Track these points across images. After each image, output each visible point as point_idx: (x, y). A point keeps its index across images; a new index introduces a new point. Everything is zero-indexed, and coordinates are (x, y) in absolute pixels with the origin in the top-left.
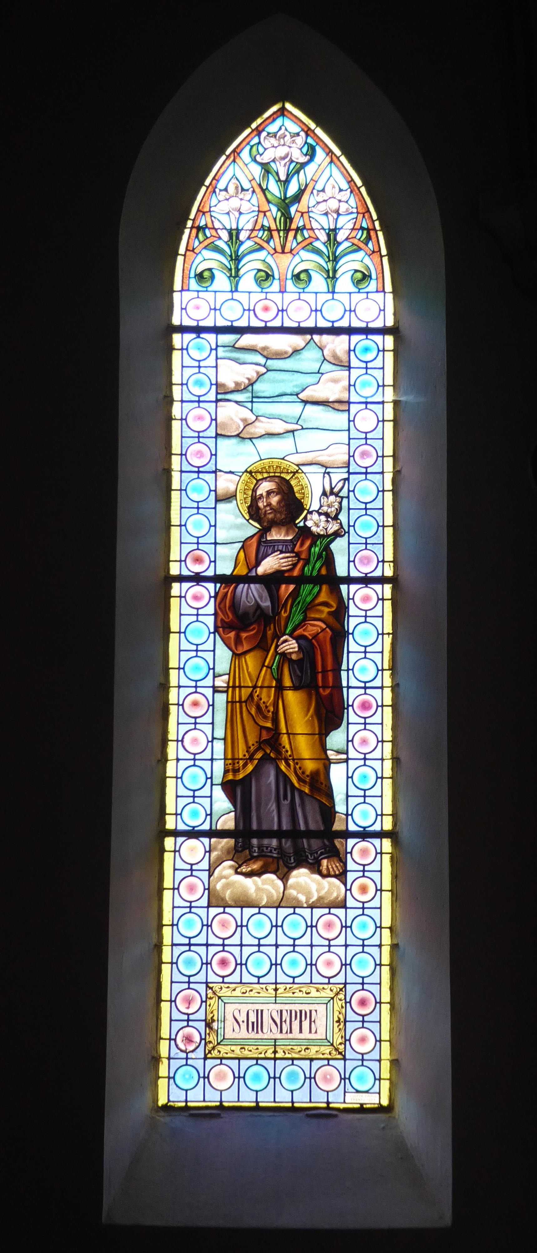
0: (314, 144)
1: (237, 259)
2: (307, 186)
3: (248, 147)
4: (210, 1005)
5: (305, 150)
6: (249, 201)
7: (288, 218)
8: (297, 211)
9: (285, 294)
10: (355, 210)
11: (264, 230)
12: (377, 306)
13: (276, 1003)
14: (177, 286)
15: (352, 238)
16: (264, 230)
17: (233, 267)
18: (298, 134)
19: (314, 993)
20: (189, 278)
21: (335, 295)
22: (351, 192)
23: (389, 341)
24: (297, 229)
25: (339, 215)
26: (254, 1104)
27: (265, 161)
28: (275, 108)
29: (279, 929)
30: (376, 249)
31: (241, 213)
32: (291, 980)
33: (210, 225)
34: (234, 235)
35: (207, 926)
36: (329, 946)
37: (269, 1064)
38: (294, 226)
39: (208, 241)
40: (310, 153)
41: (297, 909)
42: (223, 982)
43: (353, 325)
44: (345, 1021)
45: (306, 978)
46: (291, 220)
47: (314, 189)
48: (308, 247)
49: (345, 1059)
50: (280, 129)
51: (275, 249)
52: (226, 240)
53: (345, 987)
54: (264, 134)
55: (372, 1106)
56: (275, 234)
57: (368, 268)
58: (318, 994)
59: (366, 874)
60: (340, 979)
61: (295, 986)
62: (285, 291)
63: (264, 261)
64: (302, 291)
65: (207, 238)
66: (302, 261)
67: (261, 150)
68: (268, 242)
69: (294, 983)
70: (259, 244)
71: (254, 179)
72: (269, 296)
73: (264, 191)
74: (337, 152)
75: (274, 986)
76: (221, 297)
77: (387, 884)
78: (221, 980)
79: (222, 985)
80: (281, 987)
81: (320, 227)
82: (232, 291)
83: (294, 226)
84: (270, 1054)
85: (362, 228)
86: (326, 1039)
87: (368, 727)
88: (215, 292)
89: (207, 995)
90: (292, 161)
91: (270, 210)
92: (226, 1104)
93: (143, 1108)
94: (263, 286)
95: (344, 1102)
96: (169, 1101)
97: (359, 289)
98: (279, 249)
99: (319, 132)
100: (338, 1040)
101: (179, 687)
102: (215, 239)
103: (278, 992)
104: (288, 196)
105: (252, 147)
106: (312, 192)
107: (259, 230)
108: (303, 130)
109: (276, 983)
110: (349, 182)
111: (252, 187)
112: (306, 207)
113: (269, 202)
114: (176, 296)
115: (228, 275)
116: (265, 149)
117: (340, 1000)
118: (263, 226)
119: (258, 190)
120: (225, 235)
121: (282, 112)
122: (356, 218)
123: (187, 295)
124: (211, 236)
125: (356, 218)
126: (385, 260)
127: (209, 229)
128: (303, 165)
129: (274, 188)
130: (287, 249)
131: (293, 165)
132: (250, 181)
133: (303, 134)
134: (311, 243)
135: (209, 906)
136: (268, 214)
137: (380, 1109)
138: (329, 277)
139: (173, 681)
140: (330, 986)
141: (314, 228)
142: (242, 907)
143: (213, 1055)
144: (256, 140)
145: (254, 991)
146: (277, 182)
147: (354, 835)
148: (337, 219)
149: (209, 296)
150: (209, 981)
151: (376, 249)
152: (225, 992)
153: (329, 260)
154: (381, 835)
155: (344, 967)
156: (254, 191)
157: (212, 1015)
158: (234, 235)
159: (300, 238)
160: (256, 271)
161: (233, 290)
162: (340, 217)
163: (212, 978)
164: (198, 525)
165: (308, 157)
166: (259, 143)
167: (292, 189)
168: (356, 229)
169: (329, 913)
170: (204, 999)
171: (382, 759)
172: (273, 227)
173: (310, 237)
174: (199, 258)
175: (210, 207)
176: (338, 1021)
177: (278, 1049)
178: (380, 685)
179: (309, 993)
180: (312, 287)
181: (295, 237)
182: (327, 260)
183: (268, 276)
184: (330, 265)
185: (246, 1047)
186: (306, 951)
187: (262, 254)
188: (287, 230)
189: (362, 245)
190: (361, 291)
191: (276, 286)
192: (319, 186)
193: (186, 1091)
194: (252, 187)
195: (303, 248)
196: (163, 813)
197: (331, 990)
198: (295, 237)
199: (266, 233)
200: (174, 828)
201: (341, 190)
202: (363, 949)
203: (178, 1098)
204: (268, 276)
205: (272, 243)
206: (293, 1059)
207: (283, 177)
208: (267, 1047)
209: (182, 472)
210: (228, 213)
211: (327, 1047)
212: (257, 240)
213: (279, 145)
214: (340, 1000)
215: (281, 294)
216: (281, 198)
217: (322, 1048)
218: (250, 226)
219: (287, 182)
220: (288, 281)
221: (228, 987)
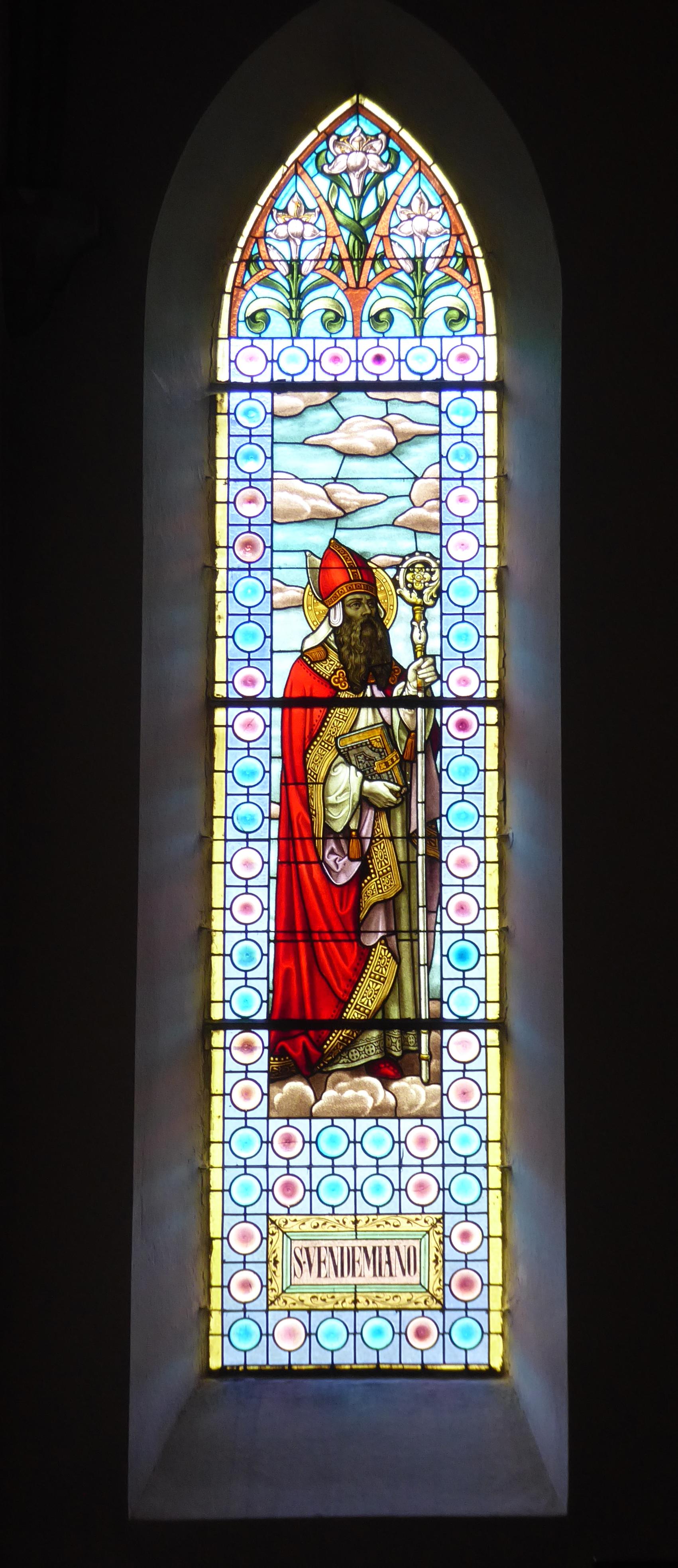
0: (398, 149)
4: (271, 1243)
5: (385, 157)
6: (439, 221)
7: (365, 245)
8: (374, 234)
9: (360, 341)
10: (323, 234)
11: (458, 257)
12: (480, 355)
13: (356, 1239)
14: (223, 331)
15: (445, 267)
16: (458, 257)
17: (417, 305)
18: (376, 137)
19: (404, 1226)
20: (238, 321)
21: (423, 340)
22: (445, 210)
23: (491, 397)
24: (374, 259)
25: (303, 240)
26: (462, 1367)
27: (336, 171)
28: (347, 105)
29: (358, 1146)
31: (427, 237)
32: (419, 1210)
34: (295, 266)
35: (443, 1142)
36: (378, 1166)
37: (348, 1317)
39: (388, 272)
40: (392, 160)
41: (380, 1120)
42: (289, 1214)
43: (318, 379)
44: (267, 1262)
45: (393, 1207)
46: (368, 245)
47: (397, 203)
48: (388, 280)
49: (443, 1310)
50: (355, 130)
51: (347, 284)
52: (285, 274)
53: (443, 1218)
54: (333, 138)
55: (366, 1367)
56: (347, 264)
58: (409, 1227)
59: (467, 1074)
60: (437, 1207)
61: (380, 1217)
62: (361, 337)
64: (381, 335)
65: (261, 270)
66: (381, 298)
67: (330, 158)
68: (462, 273)
69: (378, 1214)
71: (321, 195)
72: (340, 343)
73: (332, 211)
74: (427, 159)
75: (353, 1218)
76: (279, 345)
77: (495, 1086)
78: (285, 1211)
79: (288, 1218)
80: (362, 1219)
81: (405, 256)
82: (292, 338)
83: (371, 253)
84: (348, 1304)
85: (331, 257)
86: (420, 1284)
87: (250, 890)
88: (272, 339)
89: (268, 1229)
90: (368, 171)
91: (341, 235)
92: (472, 1367)
93: (179, 1374)
94: (331, 331)
95: (444, 1363)
96: (355, 1363)
97: (454, 332)
98: (352, 284)
99: (405, 135)
100: (435, 1285)
101: (226, 840)
102: (395, 271)
103: (358, 1225)
104: (363, 215)
105: (318, 155)
106: (395, 209)
107: (327, 260)
108: (383, 132)
109: (355, 1214)
110: (441, 196)
111: (319, 206)
113: (339, 224)
114: (222, 346)
115: (411, 317)
116: (335, 158)
117: (438, 1233)
118: (331, 254)
119: (325, 208)
120: (283, 268)
121: (357, 110)
122: (325, 243)
123: (236, 344)
124: (391, 266)
125: (325, 243)
127: (389, 259)
128: (382, 177)
129: (346, 206)
130: (363, 283)
132: (316, 198)
133: (382, 137)
134: (392, 275)
135: (442, 1118)
136: (338, 239)
137: (490, 1373)
138: (291, 318)
139: (218, 833)
140: (424, 1216)
141: (397, 256)
142: (355, 1118)
143: (277, 1307)
144: (323, 146)
145: (328, 1225)
146: (349, 198)
147: (450, 1025)
148: (301, 246)
149: (266, 345)
150: (270, 1212)
152: (292, 1226)
153: (416, 296)
154: (485, 1024)
155: (441, 1192)
156: (321, 212)
157: (274, 1255)
158: (419, 263)
159: (378, 268)
160: (446, 310)
161: (294, 335)
162: (305, 243)
163: (274, 1208)
164: (249, 638)
165: (389, 166)
166: (328, 149)
168: (447, 257)
169: (422, 1125)
170: (265, 1236)
171: (224, 932)
172: (345, 255)
173: (391, 266)
174: (250, 296)
175: (390, 228)
176: (276, 1262)
177: (360, 1298)
178: (267, 837)
179: (397, 1226)
180: (395, 331)
181: (373, 267)
182: (413, 296)
183: (338, 317)
184: (417, 301)
185: (320, 1296)
186: (348, 1173)
187: (331, 290)
188: (362, 260)
190: (456, 334)
191: (471, 328)
192: (404, 201)
193: (245, 1352)
194: (319, 206)
195: (382, 282)
196: (208, 1002)
197: (426, 1222)
198: (373, 267)
199: (336, 263)
200: (221, 1017)
201: (431, 206)
202: (245, 1171)
203: (234, 1359)
204: (338, 317)
205: (343, 276)
206: (377, 1310)
207: (357, 191)
208: (346, 1295)
209: (229, 569)
210: (412, 237)
211: (420, 1295)
212: (324, 272)
213: (352, 151)
214: (438, 1233)
215: (354, 341)
216: (354, 219)
217: (416, 1296)
218: (439, 252)
219: (362, 198)
220: (240, 324)
221: (295, 1220)
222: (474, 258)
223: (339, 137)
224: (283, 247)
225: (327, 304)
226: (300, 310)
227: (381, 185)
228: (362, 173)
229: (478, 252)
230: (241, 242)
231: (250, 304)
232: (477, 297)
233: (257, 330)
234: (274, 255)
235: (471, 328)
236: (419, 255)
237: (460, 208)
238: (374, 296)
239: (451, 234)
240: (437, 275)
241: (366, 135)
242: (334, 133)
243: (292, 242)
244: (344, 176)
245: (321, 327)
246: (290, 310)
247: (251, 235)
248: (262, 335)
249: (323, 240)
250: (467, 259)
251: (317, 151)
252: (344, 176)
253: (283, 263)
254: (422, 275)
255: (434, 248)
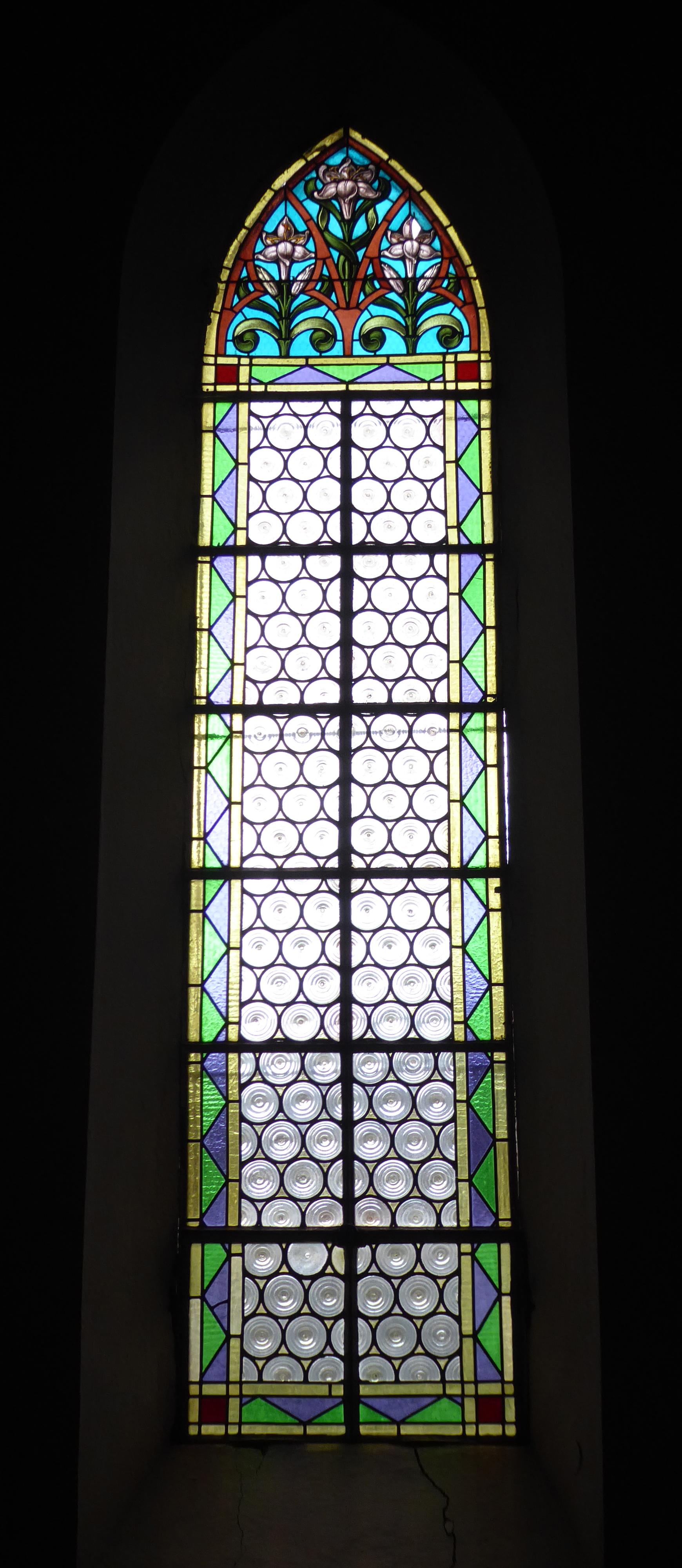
0: (388, 178)
1: (287, 317)
2: (378, 226)
3: (302, 184)
5: (376, 184)
17: (409, 323)
30: (469, 300)
33: (254, 278)
34: (283, 287)
38: (361, 275)
39: (375, 296)
51: (337, 304)
52: (400, 291)
54: (323, 168)
56: (337, 285)
57: (459, 323)
63: (324, 318)
67: (320, 185)
70: (316, 298)
73: (321, 232)
83: (361, 275)
85: (321, 278)
90: (358, 197)
99: (280, 182)
105: (307, 183)
107: (317, 281)
108: (372, 163)
111: (309, 229)
112: (377, 250)
119: (315, 232)
121: (345, 143)
126: (483, 313)
129: (335, 228)
130: (353, 303)
131: (360, 202)
138: (280, 338)
151: (469, 300)
156: (311, 235)
166: (318, 177)
167: (360, 228)
168: (314, 280)
172: (335, 276)
187: (321, 311)
188: (352, 281)
189: (450, 296)
198: (363, 289)
212: (315, 294)
222: (468, 279)
223: (329, 167)
224: (272, 269)
225: (316, 324)
226: (289, 331)
227: (371, 212)
228: (351, 200)
229: (472, 272)
230: (228, 262)
231: (239, 325)
232: (472, 316)
233: (373, 348)
234: (263, 276)
235: (338, 349)
236: (410, 275)
237: (451, 231)
238: (366, 315)
239: (316, 258)
240: (303, 298)
241: (355, 166)
242: (323, 163)
243: (407, 261)
244: (335, 202)
245: (437, 343)
246: (407, 327)
247: (238, 258)
248: (378, 353)
249: (313, 261)
250: (237, 284)
251: (307, 178)
252: (335, 202)
253: (399, 282)
254: (413, 296)
255: (427, 269)
